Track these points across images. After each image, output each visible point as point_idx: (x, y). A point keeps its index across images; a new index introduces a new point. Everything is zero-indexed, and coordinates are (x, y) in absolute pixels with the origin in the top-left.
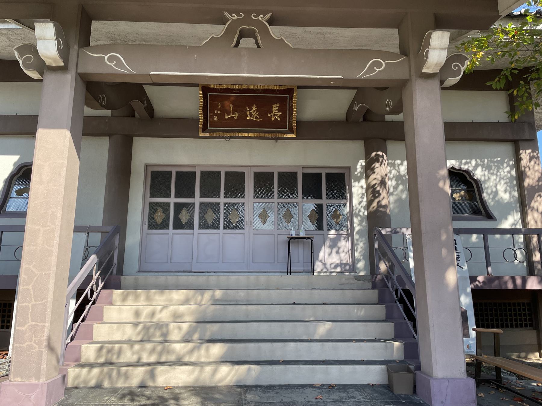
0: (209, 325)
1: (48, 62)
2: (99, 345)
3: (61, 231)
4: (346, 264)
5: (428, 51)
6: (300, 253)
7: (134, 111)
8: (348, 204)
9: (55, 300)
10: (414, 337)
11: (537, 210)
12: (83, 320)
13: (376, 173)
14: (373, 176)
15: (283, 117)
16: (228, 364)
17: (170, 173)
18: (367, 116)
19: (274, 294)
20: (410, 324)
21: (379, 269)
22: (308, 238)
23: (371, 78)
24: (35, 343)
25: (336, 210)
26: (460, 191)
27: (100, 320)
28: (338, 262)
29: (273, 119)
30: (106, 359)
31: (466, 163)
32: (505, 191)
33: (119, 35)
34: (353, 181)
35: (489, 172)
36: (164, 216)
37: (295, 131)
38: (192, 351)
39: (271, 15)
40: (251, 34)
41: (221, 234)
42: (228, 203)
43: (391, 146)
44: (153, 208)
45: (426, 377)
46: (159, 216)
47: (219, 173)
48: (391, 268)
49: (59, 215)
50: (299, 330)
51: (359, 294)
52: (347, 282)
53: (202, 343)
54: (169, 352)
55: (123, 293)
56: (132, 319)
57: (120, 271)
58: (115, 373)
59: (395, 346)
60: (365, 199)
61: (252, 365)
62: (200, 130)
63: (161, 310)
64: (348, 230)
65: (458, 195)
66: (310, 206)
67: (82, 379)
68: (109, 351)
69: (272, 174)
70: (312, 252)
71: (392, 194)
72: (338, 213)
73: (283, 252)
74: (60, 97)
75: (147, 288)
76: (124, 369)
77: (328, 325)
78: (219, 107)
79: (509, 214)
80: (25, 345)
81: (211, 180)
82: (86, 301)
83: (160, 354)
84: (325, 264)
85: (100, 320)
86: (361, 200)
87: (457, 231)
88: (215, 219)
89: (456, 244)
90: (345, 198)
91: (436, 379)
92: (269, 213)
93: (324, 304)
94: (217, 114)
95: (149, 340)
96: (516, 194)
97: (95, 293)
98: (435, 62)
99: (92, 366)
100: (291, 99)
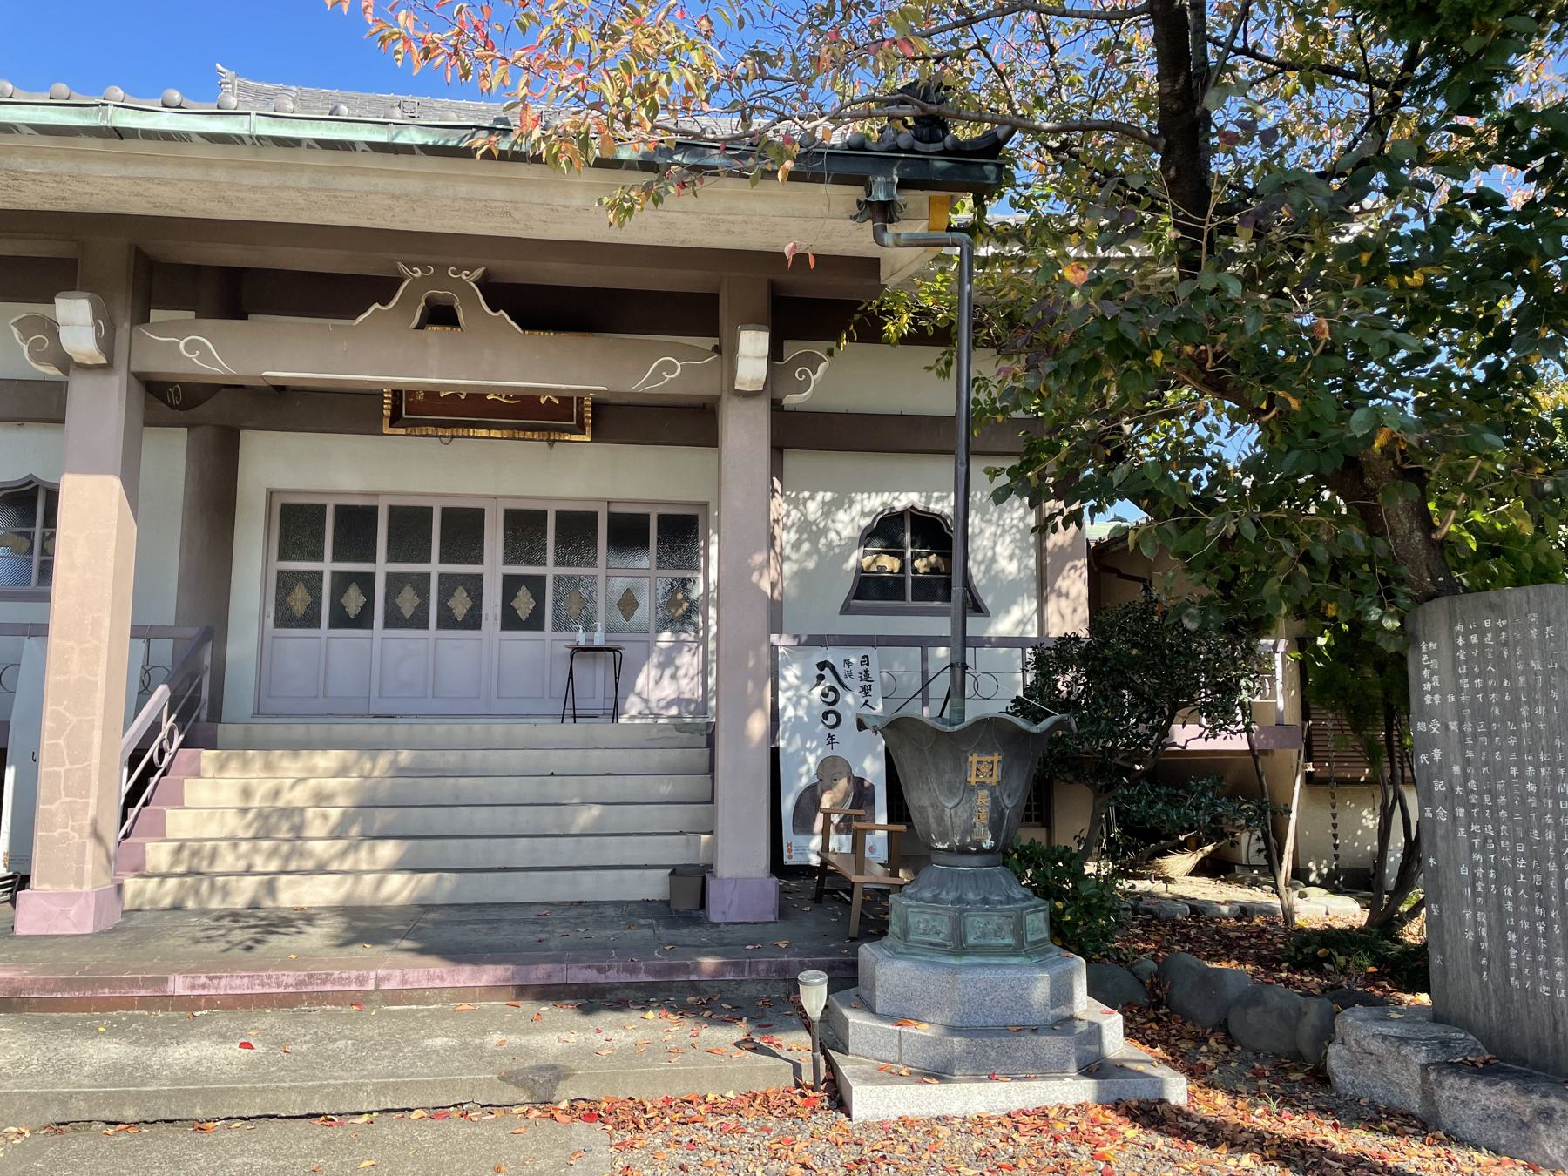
0: (377, 812)
4: (689, 701)
6: (594, 678)
8: (701, 577)
9: (103, 762)
11: (1067, 595)
12: (146, 804)
19: (515, 758)
22: (609, 650)
24: (73, 829)
26: (930, 554)
27: (178, 802)
31: (939, 500)
32: (1011, 557)
35: (982, 519)
36: (309, 599)
37: (588, 429)
38: (343, 854)
44: (286, 582)
49: (106, 622)
50: (547, 819)
54: (302, 854)
57: (216, 714)
58: (205, 886)
62: (386, 422)
63: (293, 786)
64: (697, 632)
65: (924, 561)
67: (148, 895)
68: (194, 854)
74: (101, 407)
75: (265, 746)
76: (220, 880)
77: (596, 811)
79: (1014, 602)
80: (56, 834)
81: (410, 526)
82: (151, 769)
83: (287, 858)
84: (646, 701)
85: (178, 802)
90: (697, 568)
96: (1032, 562)
99: (164, 876)
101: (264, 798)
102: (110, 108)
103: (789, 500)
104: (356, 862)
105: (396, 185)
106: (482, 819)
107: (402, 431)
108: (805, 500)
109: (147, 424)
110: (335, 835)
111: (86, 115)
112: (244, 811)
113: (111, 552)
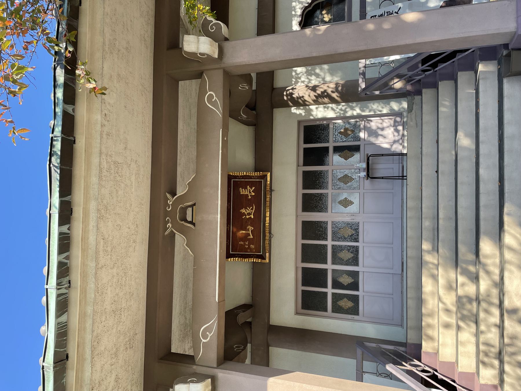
2: (481, 366)
4: (395, 121)
5: (200, 54)
6: (383, 168)
10: (473, 51)
12: (454, 381)
13: (304, 95)
14: (306, 98)
15: (252, 184)
16: (502, 235)
18: (251, 107)
19: (428, 192)
20: (459, 56)
21: (401, 89)
22: (368, 159)
23: (222, 103)
25: (340, 133)
27: (453, 365)
28: (392, 129)
29: (253, 194)
30: (495, 358)
33: (181, 331)
34: (312, 118)
36: (345, 299)
37: (265, 173)
38: (488, 273)
39: (168, 193)
40: (184, 211)
41: (364, 244)
42: (333, 237)
43: (279, 83)
44: (337, 309)
45: (515, 39)
46: (346, 304)
47: (303, 245)
48: (400, 77)
50: (466, 167)
52: (414, 120)
53: (480, 262)
55: (425, 340)
56: (453, 332)
58: (510, 349)
59: (482, 70)
60: (330, 105)
61: (503, 212)
62: (263, 261)
63: (443, 303)
65: (326, 16)
66: (336, 159)
68: (486, 354)
70: (383, 155)
71: (323, 79)
72: (342, 130)
75: (419, 317)
76: (506, 340)
78: (242, 243)
81: (310, 253)
82: (434, 377)
83: (491, 304)
84: (395, 142)
85: (453, 365)
86: (330, 109)
87: (363, 15)
88: (349, 250)
89: (376, 16)
91: (517, 28)
92: (342, 198)
93: (437, 142)
94: (249, 245)
95: (476, 316)
97: (425, 369)
98: (210, 47)
99: (502, 372)
100: (235, 177)
101: (450, 317)
102: (44, 364)
103: (297, 82)
104: (494, 264)
105: (93, 216)
106: (466, 203)
107: (267, 254)
108: (296, 74)
109: (267, 365)
110: (475, 279)
112: (459, 328)
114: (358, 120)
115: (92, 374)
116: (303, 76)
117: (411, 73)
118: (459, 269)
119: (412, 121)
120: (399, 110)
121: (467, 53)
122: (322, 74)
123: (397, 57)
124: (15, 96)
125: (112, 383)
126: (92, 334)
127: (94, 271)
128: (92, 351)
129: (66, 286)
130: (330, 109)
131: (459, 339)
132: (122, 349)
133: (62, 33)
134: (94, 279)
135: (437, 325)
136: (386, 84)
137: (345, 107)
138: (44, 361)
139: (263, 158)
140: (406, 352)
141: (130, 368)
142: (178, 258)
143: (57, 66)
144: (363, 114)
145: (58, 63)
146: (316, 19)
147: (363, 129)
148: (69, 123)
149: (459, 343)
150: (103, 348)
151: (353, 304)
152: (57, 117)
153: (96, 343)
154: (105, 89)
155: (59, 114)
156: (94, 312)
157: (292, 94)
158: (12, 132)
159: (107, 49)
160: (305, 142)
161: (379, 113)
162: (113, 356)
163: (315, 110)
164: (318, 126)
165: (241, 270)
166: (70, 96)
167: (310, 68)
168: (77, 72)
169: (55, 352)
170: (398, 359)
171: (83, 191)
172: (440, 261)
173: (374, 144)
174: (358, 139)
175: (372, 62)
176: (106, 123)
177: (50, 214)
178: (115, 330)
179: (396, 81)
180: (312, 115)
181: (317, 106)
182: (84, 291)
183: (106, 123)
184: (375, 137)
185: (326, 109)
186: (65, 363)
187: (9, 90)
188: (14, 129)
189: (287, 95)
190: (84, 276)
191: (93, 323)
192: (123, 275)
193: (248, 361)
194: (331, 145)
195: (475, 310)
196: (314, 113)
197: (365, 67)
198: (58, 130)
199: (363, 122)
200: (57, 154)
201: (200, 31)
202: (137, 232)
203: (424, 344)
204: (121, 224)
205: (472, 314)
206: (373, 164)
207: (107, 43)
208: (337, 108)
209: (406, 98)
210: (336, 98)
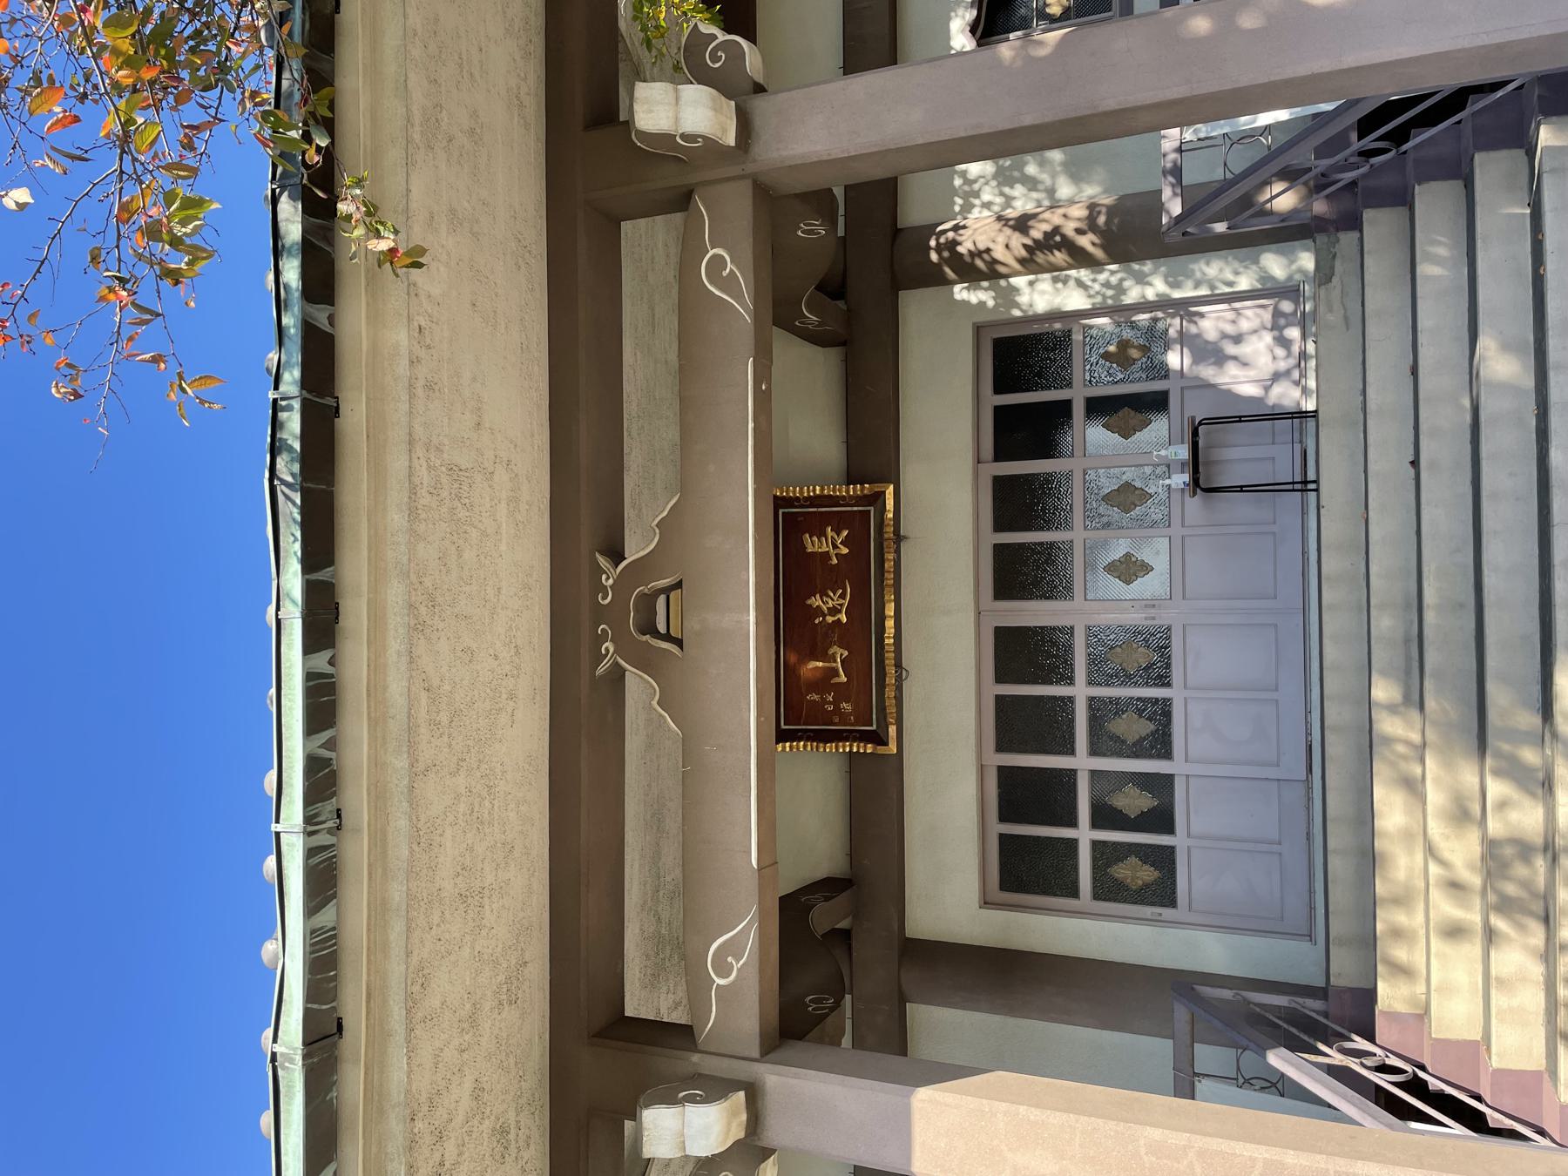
1: (738, 1133)
3: (1205, 1134)
4: (1277, 314)
5: (683, 136)
6: (1241, 457)
7: (834, 932)
10: (1521, 87)
13: (991, 246)
14: (999, 253)
15: (839, 522)
17: (1004, 839)
18: (833, 288)
19: (1386, 526)
20: (1476, 105)
21: (1294, 212)
22: (1195, 433)
25: (1107, 356)
27: (1476, 1050)
29: (845, 551)
34: (1017, 313)
36: (1133, 860)
37: (877, 488)
39: (601, 553)
41: (1187, 693)
42: (1089, 673)
43: (913, 213)
44: (1108, 889)
46: (1136, 873)
47: (999, 699)
48: (1290, 175)
49: (1156, 1134)
51: (1380, 266)
53: (1555, 735)
55: (1384, 979)
56: (1474, 949)
59: (1550, 143)
60: (1073, 273)
62: (881, 750)
63: (1442, 862)
66: (1097, 436)
69: (999, 549)
70: (1240, 419)
71: (1051, 192)
72: (1112, 348)
73: (1240, 506)
75: (1368, 907)
78: (816, 697)
81: (1021, 724)
82: (1416, 1086)
84: (1276, 377)
85: (1476, 1050)
86: (1072, 283)
88: (1140, 712)
92: (1117, 551)
94: (836, 703)
95: (1545, 898)
97: (1388, 1062)
98: (710, 113)
101: (1465, 905)
102: (278, 1048)
103: (967, 208)
105: (396, 622)
107: (892, 730)
109: (903, 1051)
111: (290, 1087)
112: (1490, 935)
113: (1035, 1114)
114: (1160, 314)
115: (410, 1072)
116: (987, 188)
117: (1325, 163)
118: (1489, 761)
119: (1331, 311)
120: (1290, 278)
121: (1500, 94)
122: (1045, 178)
123: (1282, 115)
124: (177, 283)
125: (466, 1103)
126: (407, 963)
127: (406, 782)
128: (408, 1011)
129: (330, 824)
130: (1072, 283)
131: (1493, 972)
132: (487, 1006)
133: (291, 95)
134: (405, 804)
135: (1422, 932)
136: (1247, 201)
137: (1119, 276)
138: (275, 1040)
139: (872, 441)
140: (1332, 1013)
141: (512, 1060)
142: (634, 744)
143: (281, 194)
144: (1177, 294)
145: (282, 182)
146: (1023, 11)
147: (1175, 341)
148: (320, 357)
149: (1493, 983)
150: (437, 1003)
151: (1157, 874)
152: (286, 340)
153: (416, 988)
154: (422, 251)
155: (292, 331)
156: (410, 896)
157: (955, 243)
158: (176, 387)
159: (417, 137)
160: (999, 389)
161: (1227, 290)
162: (466, 1025)
163: (1026, 290)
164: (1037, 339)
165: (817, 775)
166: (321, 281)
167: (1008, 163)
168: (342, 207)
169: (308, 1014)
170: (1303, 1033)
171: (365, 553)
172: (1431, 735)
173: (1214, 386)
174: (1164, 372)
175: (1202, 135)
176: (422, 353)
177: (278, 622)
178: (467, 951)
179: (1278, 187)
180: (1017, 306)
181: (1032, 277)
182: (380, 840)
183: (422, 353)
184: (1215, 363)
185: (1060, 285)
186: (335, 1045)
187: (162, 268)
188: (181, 378)
189: (939, 249)
190: (379, 797)
191: (409, 930)
192: (484, 793)
193: (846, 1041)
194: (1077, 395)
195: (1541, 882)
196: (1023, 299)
197: (1180, 150)
198: (292, 377)
199: (1177, 321)
200: (290, 449)
201: (677, 68)
202: (518, 668)
203: (1382, 988)
204: (474, 646)
205: (1535, 895)
206: (1209, 447)
207: (417, 118)
208: (1094, 280)
209: (1309, 242)
210: (1090, 248)
